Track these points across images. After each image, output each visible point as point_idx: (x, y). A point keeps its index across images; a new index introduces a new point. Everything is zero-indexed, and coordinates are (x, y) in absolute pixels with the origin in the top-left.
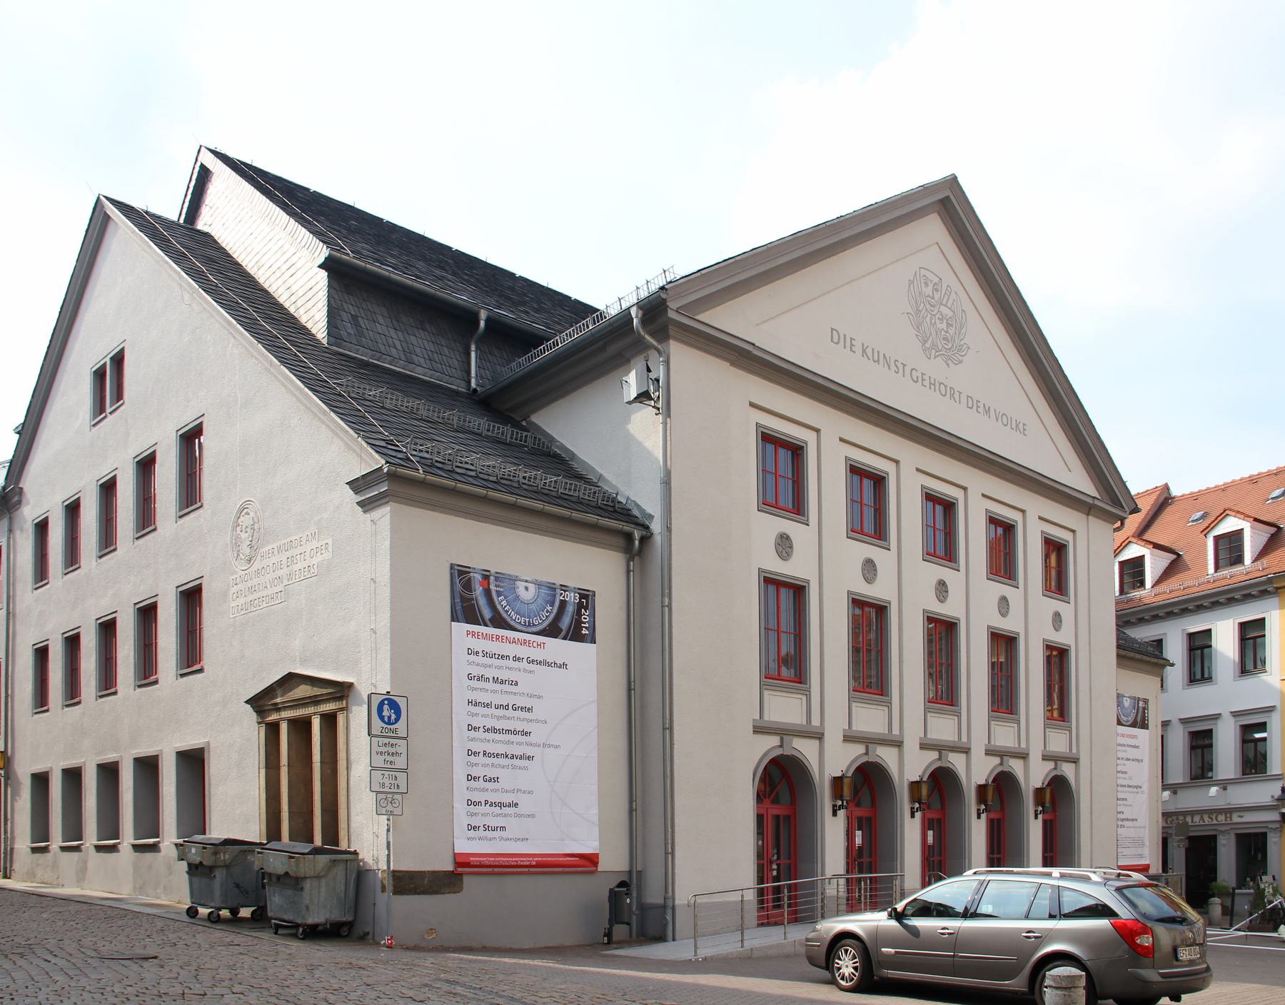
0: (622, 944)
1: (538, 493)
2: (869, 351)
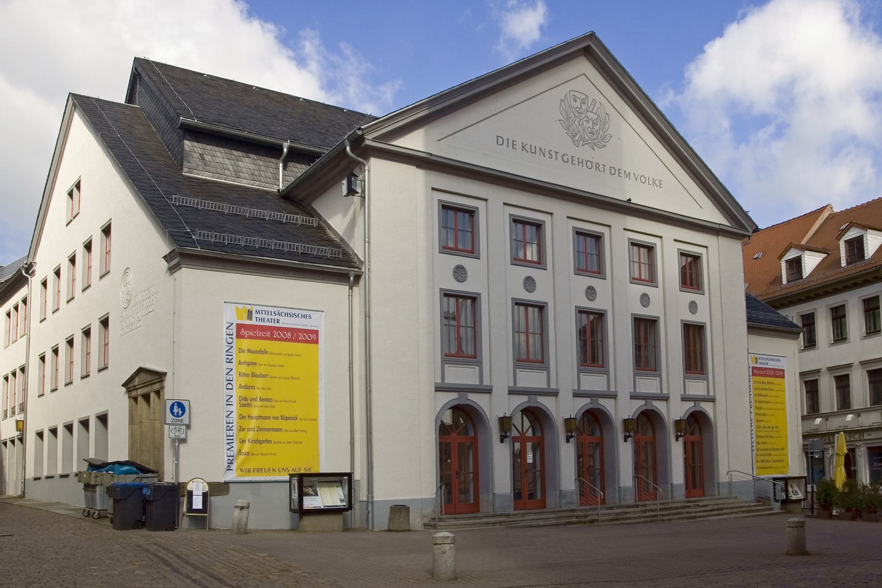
1: (291, 255)
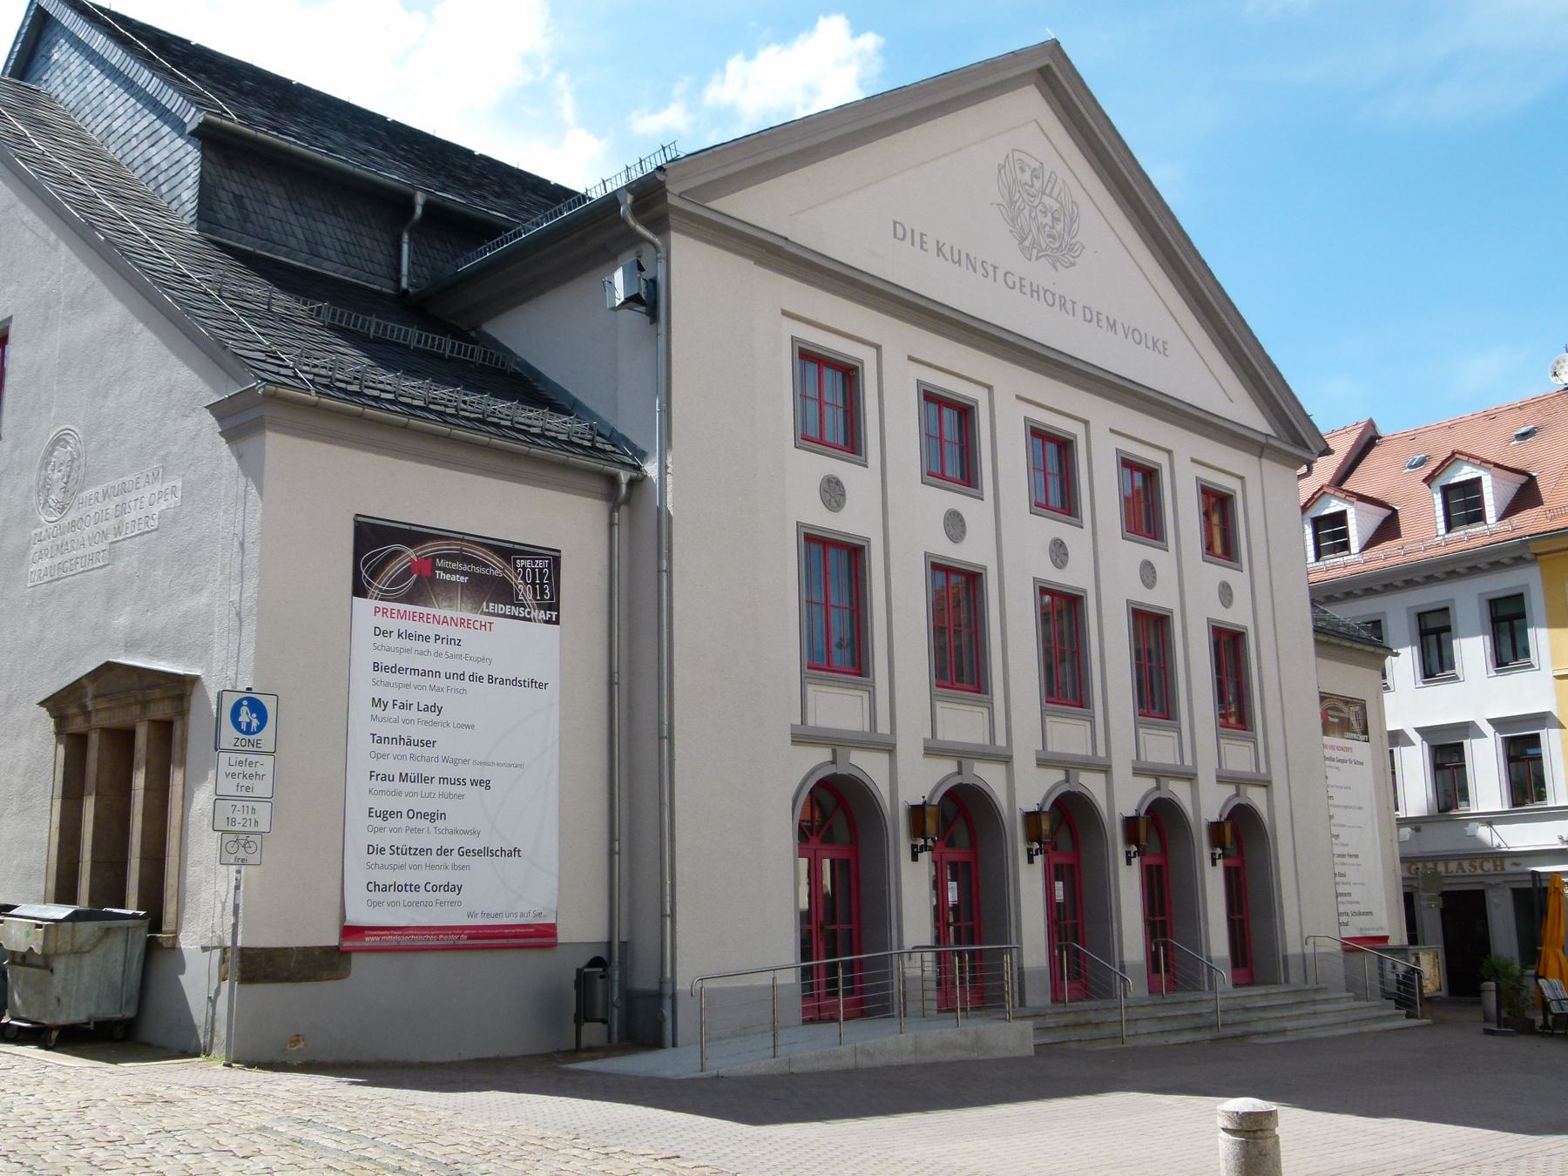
0: (594, 1052)
2: (946, 250)
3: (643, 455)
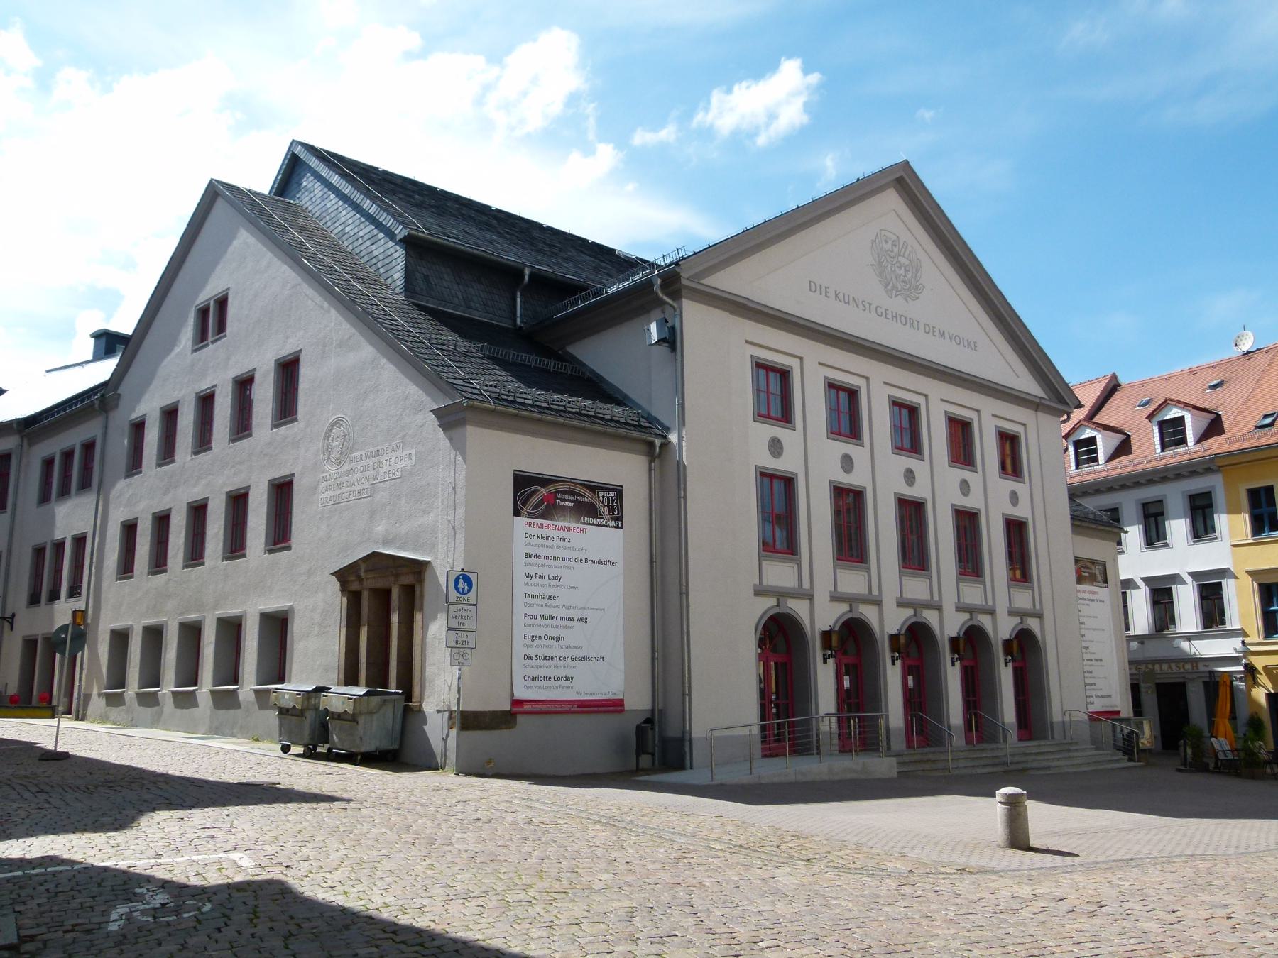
0: (647, 771)
2: (841, 296)
3: (668, 429)
